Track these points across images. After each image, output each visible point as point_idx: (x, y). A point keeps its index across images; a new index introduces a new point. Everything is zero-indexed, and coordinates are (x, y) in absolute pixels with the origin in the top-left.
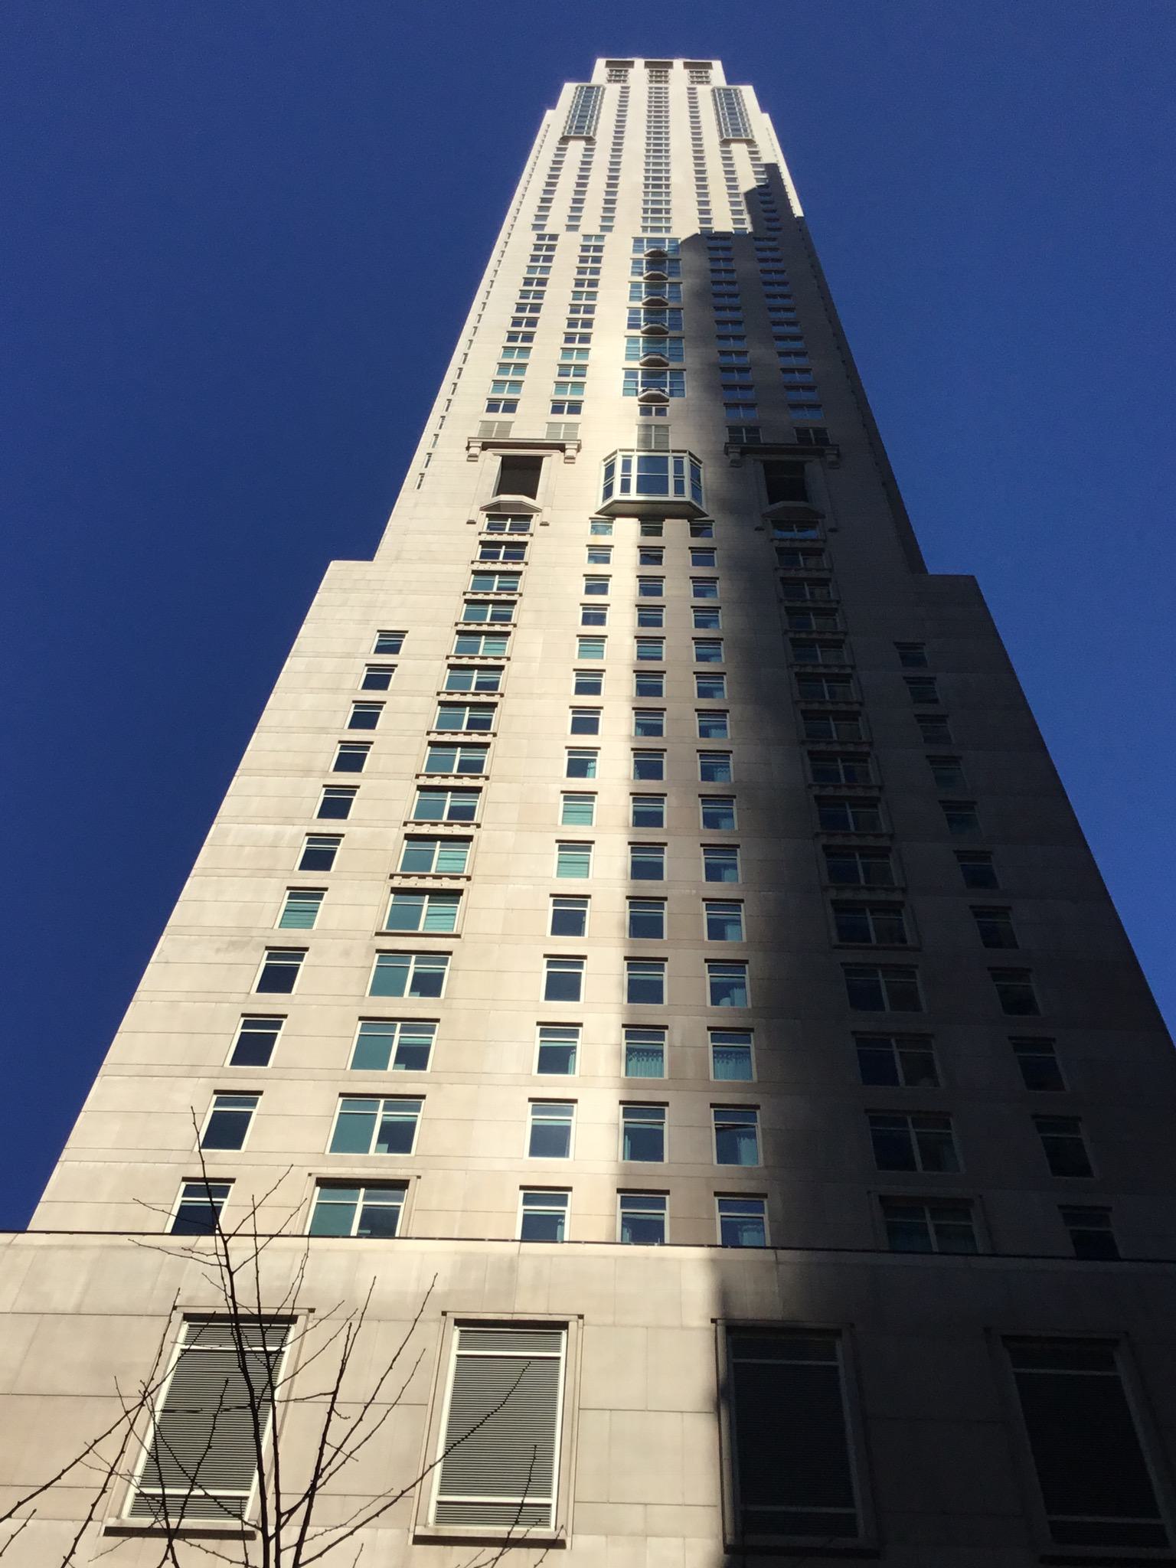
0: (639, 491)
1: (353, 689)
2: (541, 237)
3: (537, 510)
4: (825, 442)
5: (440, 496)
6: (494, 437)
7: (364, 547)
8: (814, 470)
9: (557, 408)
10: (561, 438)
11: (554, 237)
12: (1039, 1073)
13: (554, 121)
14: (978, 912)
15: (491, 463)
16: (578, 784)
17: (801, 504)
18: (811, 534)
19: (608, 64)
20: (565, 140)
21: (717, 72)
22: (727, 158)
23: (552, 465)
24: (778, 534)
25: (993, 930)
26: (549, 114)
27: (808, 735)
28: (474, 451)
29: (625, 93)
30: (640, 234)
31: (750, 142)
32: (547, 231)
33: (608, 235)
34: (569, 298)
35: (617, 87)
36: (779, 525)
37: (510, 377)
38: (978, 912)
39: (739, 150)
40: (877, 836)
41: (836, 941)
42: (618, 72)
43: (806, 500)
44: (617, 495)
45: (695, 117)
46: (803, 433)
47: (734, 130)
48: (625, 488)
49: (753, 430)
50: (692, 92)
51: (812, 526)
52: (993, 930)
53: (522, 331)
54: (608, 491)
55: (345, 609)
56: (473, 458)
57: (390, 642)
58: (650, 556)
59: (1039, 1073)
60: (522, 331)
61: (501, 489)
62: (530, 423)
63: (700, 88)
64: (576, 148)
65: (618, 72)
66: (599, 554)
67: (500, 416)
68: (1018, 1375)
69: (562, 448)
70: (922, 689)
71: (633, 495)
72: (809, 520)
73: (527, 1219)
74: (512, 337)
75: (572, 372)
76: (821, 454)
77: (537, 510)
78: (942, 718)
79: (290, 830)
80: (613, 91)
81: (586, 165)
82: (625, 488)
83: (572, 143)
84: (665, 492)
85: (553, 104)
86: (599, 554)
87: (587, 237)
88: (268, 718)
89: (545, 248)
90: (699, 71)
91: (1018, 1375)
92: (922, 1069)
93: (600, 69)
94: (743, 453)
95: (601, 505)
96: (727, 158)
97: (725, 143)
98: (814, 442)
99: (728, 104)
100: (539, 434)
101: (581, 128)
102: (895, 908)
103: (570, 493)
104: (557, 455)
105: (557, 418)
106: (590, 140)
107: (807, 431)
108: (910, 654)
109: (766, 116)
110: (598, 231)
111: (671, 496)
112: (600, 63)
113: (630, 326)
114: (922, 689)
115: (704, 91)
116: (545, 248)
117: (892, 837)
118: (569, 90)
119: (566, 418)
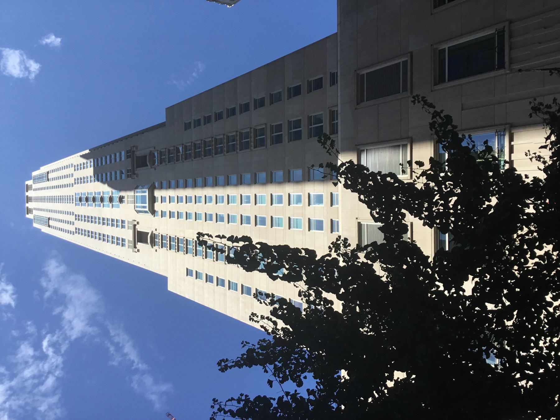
0: (146, 203)
1: (201, 282)
2: (76, 233)
3: (152, 232)
4: (130, 150)
5: (147, 258)
6: (132, 245)
7: (164, 280)
8: (139, 153)
9: (123, 227)
10: (131, 225)
11: (76, 229)
12: (297, 91)
13: (45, 229)
14: (256, 108)
15: (140, 245)
16: (268, 221)
17: (147, 157)
18: (156, 154)
19: (28, 214)
20: (49, 226)
21: (29, 182)
22: (53, 179)
23: (139, 228)
24: (156, 164)
25: (260, 103)
26: (43, 230)
27: (234, 151)
28: (136, 250)
29: (35, 209)
30: (74, 204)
31: (48, 173)
32: (74, 231)
33: (75, 213)
34: (110, 227)
35: (34, 211)
36: (154, 164)
37: (121, 242)
38: (256, 108)
39: (51, 176)
40: (251, 133)
41: (264, 147)
42: (29, 211)
43: (146, 156)
44: (147, 209)
45: (44, 188)
46: (128, 157)
47: (46, 177)
48: (145, 207)
49: (128, 171)
50: (35, 190)
51: (154, 154)
52: (260, 103)
53: (103, 237)
54: (146, 212)
55: (180, 286)
56: (138, 251)
57: (189, 272)
58: (163, 199)
59: (297, 91)
60: (103, 237)
61: (146, 242)
62: (128, 234)
63: (33, 187)
64: (51, 223)
65: (29, 211)
66: (163, 214)
67: (126, 243)
68: (449, 80)
69: (135, 226)
70: (198, 123)
71: (147, 205)
72: (152, 155)
73: (317, 229)
74: (104, 240)
75: (113, 223)
76: (134, 152)
77: (152, 232)
78: (271, 95)
79: (241, 299)
80: (35, 212)
81: (55, 220)
82: (145, 207)
83: (50, 224)
84: (145, 196)
85: (40, 230)
86: (163, 214)
87: (76, 219)
88: (211, 306)
89: (78, 231)
90: (28, 188)
91: (449, 80)
92: (298, 124)
93: (29, 216)
94: (134, 174)
95: (150, 214)
96: (53, 179)
97: (48, 180)
98: (130, 154)
99: (39, 179)
100: (131, 232)
101: (47, 222)
102: (256, 131)
103: (148, 223)
104: (137, 227)
105: (126, 227)
106: (49, 219)
107: (127, 156)
108: (187, 126)
109: (41, 168)
110: (74, 216)
111: (147, 194)
112: (27, 216)
113: (100, 206)
114: (198, 123)
115: (34, 186)
116: (78, 231)
117: (251, 128)
118: (35, 225)
119: (126, 224)
